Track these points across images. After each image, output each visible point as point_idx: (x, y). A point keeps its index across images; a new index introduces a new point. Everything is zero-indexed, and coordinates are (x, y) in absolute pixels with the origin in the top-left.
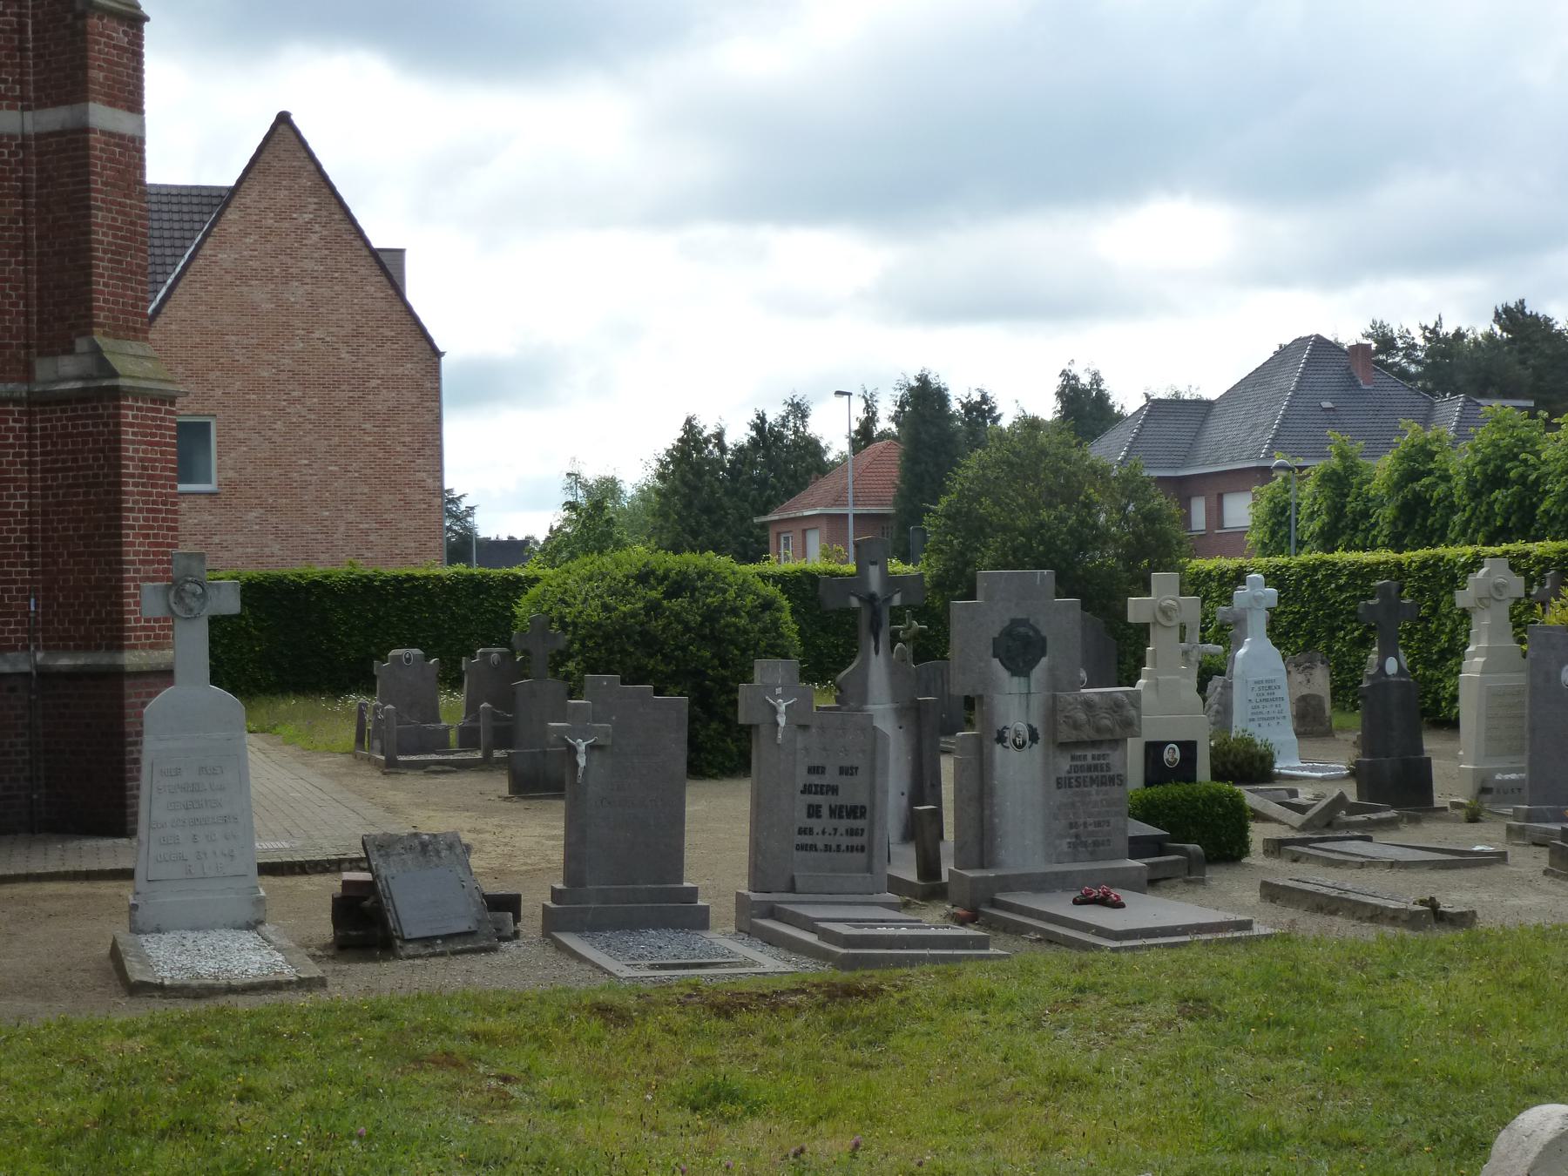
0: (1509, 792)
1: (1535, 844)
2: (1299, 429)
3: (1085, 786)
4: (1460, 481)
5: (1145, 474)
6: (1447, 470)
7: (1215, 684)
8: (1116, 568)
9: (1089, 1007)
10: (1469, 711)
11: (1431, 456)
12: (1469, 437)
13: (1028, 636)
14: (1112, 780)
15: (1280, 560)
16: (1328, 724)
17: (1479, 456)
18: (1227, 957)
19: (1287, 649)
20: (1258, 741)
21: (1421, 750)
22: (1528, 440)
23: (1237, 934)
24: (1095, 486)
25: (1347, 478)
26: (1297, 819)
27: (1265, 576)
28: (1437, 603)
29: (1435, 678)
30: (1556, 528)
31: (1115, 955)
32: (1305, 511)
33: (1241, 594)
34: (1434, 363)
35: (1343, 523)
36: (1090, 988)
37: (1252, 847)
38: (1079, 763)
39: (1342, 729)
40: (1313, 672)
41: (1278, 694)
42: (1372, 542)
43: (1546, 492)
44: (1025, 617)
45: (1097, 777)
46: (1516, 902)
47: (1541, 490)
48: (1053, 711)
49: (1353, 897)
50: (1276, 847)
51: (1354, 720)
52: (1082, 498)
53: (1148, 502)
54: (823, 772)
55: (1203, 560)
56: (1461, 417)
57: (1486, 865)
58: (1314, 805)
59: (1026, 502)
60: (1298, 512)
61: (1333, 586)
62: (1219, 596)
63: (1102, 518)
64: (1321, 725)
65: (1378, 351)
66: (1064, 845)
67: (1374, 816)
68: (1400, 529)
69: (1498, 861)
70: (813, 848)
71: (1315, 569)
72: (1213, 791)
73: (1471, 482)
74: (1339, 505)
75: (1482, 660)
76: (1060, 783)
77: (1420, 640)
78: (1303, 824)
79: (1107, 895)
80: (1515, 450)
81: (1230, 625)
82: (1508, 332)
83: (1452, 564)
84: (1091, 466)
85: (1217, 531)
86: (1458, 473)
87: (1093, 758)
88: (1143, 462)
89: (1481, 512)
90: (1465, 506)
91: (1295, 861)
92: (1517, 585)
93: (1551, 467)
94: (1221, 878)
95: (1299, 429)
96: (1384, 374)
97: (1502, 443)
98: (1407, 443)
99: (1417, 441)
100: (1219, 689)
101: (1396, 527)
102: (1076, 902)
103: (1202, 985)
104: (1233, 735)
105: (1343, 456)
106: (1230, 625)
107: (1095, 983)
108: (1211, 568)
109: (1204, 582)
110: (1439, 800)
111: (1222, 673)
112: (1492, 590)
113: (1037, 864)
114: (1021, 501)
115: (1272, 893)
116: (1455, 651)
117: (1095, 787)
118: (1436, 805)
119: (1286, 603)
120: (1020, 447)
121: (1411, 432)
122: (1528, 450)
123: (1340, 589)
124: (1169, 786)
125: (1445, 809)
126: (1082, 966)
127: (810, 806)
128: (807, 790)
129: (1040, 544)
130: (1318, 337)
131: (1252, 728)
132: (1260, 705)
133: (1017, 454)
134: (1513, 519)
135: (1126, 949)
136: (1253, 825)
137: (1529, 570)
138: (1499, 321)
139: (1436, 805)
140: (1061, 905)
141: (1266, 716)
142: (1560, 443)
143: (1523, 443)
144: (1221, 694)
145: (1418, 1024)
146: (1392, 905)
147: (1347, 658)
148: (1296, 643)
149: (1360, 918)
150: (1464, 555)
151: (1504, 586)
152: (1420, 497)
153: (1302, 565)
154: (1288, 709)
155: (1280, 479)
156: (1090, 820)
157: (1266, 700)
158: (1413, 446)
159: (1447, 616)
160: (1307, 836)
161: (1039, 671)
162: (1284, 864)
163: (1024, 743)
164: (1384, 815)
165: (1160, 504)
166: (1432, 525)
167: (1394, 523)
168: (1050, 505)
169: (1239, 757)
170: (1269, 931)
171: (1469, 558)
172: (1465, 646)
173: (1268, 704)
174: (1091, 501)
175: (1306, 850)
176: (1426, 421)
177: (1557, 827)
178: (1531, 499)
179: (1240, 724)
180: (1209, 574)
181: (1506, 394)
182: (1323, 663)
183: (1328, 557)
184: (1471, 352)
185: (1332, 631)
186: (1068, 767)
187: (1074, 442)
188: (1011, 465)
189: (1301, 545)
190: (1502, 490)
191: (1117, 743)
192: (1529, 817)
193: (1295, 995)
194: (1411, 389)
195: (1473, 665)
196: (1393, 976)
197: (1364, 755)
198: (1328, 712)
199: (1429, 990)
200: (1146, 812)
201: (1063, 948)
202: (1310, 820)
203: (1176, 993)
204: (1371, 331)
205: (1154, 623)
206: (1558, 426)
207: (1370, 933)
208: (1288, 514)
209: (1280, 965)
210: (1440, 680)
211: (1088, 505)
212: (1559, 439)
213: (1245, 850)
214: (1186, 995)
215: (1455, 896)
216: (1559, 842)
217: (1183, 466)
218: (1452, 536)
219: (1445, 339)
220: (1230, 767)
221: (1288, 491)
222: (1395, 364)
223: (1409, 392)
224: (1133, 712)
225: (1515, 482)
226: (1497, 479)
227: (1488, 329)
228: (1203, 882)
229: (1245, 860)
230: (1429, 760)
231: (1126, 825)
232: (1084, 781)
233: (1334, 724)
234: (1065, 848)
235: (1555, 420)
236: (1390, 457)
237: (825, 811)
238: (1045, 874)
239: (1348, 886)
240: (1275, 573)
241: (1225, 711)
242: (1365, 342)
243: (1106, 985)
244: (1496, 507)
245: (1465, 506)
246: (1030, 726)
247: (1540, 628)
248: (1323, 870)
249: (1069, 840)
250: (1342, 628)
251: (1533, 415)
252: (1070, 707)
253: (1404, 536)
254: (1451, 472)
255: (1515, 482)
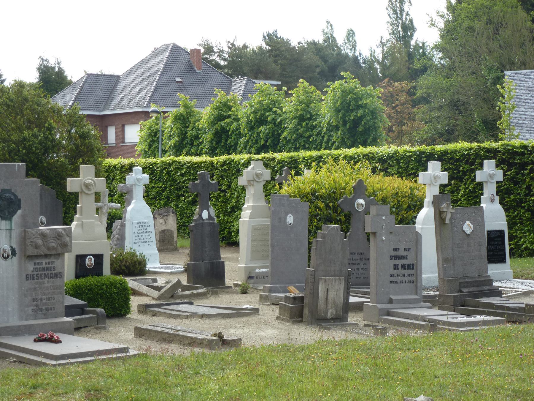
0: (262, 278)
1: (273, 304)
2: (164, 92)
3: (42, 279)
4: (243, 122)
5: (81, 113)
6: (237, 115)
7: (117, 224)
8: (64, 163)
9: (38, 396)
10: (244, 238)
11: (230, 108)
12: (248, 99)
13: (12, 199)
14: (56, 275)
15: (152, 160)
16: (175, 245)
17: (253, 109)
18: (113, 367)
19: (155, 206)
20: (138, 254)
21: (220, 258)
22: (277, 101)
23: (119, 355)
24: (53, 118)
25: (188, 118)
26: (155, 294)
27: (143, 168)
28: (230, 183)
29: (229, 221)
30: (290, 146)
31: (54, 368)
32: (166, 135)
33: (130, 178)
34: (233, 60)
35: (186, 142)
36: (39, 386)
37: (132, 309)
38: (38, 267)
39: (183, 247)
40: (168, 218)
41: (149, 229)
42: (200, 151)
43: (285, 128)
44: (9, 188)
45: (48, 274)
46: (261, 334)
47: (282, 127)
48: (24, 239)
49: (181, 333)
50: (144, 309)
51: (187, 242)
52: (46, 125)
53: (82, 128)
54: (399, 250)
55: (112, 159)
56: (245, 89)
57: (248, 315)
58: (165, 286)
59: (16, 126)
60: (163, 135)
61: (179, 174)
62: (121, 178)
63: (58, 136)
64: (172, 245)
65: (205, 53)
66: (30, 310)
67: (195, 292)
68: (214, 145)
69: (255, 313)
70: (396, 282)
71: (170, 165)
72: (111, 280)
73: (249, 122)
74: (184, 132)
75: (250, 211)
76: (27, 277)
77: (222, 202)
78: (159, 297)
79: (52, 337)
80: (271, 106)
81: (125, 193)
82: (269, 46)
83: (238, 163)
84: (51, 108)
85: (121, 144)
86: (243, 117)
87: (46, 263)
88: (80, 106)
89: (254, 138)
90: (246, 134)
91: (154, 316)
92: (267, 174)
93: (288, 115)
94: (114, 326)
95: (164, 92)
96: (207, 65)
97: (264, 103)
98: (218, 101)
99: (223, 100)
100: (119, 227)
101: (212, 144)
102: (35, 341)
103: (98, 382)
104: (125, 251)
105: (186, 107)
106: (125, 193)
107: (42, 384)
108: (116, 163)
109: (113, 171)
110: (228, 282)
111: (120, 218)
112: (255, 177)
113: (15, 321)
114: (13, 126)
115: (140, 333)
116: (238, 208)
117: (47, 279)
118: (226, 285)
119: (155, 182)
120: (13, 96)
121: (220, 95)
122: (277, 106)
123: (182, 175)
124: (88, 278)
125: (231, 287)
126: (36, 374)
127: (394, 265)
128: (392, 258)
129: (23, 149)
130: (174, 44)
131: (135, 247)
132: (140, 235)
133: (12, 100)
134: (269, 141)
135: (59, 365)
136: (132, 298)
137: (274, 167)
138: (265, 40)
139: (226, 285)
140: (28, 343)
141: (143, 241)
142: (292, 104)
143: (274, 102)
144: (120, 229)
145: (208, 397)
146: (200, 337)
147: (186, 211)
148: (160, 203)
149: (184, 344)
150: (243, 159)
151: (261, 175)
152: (224, 128)
153: (163, 163)
154: (153, 236)
155: (154, 118)
156: (44, 297)
157: (143, 233)
158: (221, 103)
159: (235, 190)
160: (161, 302)
161: (17, 218)
162: (148, 317)
163: (8, 256)
164: (200, 291)
165: (89, 129)
166: (230, 143)
167: (211, 142)
168: (29, 128)
169: (128, 263)
170: (135, 352)
171: (246, 160)
172: (243, 204)
173: (144, 234)
174: (52, 127)
175: (159, 310)
176: (228, 90)
177: (283, 295)
178: (278, 131)
179: (129, 245)
180: (115, 166)
181: (267, 77)
182: (173, 213)
183: (177, 159)
184: (251, 56)
185: (178, 197)
186: (32, 269)
187: (42, 95)
188: (8, 106)
189: (164, 152)
190: (264, 126)
191: (59, 255)
192: (271, 290)
193: (146, 386)
194: (221, 74)
195: (246, 214)
196: (197, 373)
197: (191, 260)
198: (175, 238)
199: (215, 380)
200: (76, 292)
201: (28, 365)
202: (162, 294)
203: (85, 387)
204: (202, 42)
205: (81, 192)
206: (291, 95)
207: (187, 352)
208: (158, 136)
209: (140, 370)
210: (232, 222)
211: (50, 129)
212: (292, 101)
213: (128, 311)
214: (90, 388)
215: (232, 331)
216: (283, 303)
217: (104, 109)
218: (240, 149)
219: (239, 49)
220: (123, 268)
221: (158, 124)
222: (213, 60)
223: (220, 75)
224: (68, 239)
225: (270, 123)
226: (262, 121)
227: (259, 44)
228: (105, 328)
229: (128, 316)
230: (223, 262)
231: (64, 299)
232: (41, 276)
233: (179, 245)
234: (30, 312)
235: (290, 92)
236: (209, 108)
237: (400, 267)
238: (19, 326)
239: (179, 328)
240: (149, 167)
241: (122, 238)
242: (198, 48)
243: (48, 384)
244: (261, 135)
245: (246, 134)
246: (11, 247)
247: (277, 196)
248: (167, 320)
249: (32, 308)
250: (183, 196)
251: (279, 88)
252: (33, 237)
253: (216, 148)
254: (239, 116)
255: (270, 123)
